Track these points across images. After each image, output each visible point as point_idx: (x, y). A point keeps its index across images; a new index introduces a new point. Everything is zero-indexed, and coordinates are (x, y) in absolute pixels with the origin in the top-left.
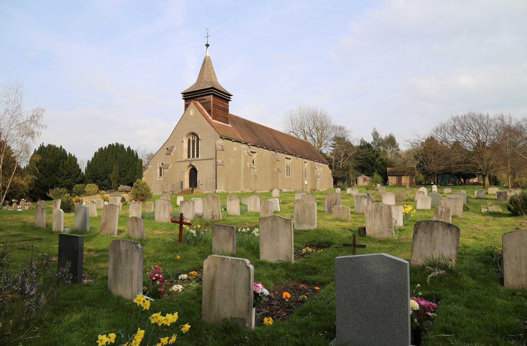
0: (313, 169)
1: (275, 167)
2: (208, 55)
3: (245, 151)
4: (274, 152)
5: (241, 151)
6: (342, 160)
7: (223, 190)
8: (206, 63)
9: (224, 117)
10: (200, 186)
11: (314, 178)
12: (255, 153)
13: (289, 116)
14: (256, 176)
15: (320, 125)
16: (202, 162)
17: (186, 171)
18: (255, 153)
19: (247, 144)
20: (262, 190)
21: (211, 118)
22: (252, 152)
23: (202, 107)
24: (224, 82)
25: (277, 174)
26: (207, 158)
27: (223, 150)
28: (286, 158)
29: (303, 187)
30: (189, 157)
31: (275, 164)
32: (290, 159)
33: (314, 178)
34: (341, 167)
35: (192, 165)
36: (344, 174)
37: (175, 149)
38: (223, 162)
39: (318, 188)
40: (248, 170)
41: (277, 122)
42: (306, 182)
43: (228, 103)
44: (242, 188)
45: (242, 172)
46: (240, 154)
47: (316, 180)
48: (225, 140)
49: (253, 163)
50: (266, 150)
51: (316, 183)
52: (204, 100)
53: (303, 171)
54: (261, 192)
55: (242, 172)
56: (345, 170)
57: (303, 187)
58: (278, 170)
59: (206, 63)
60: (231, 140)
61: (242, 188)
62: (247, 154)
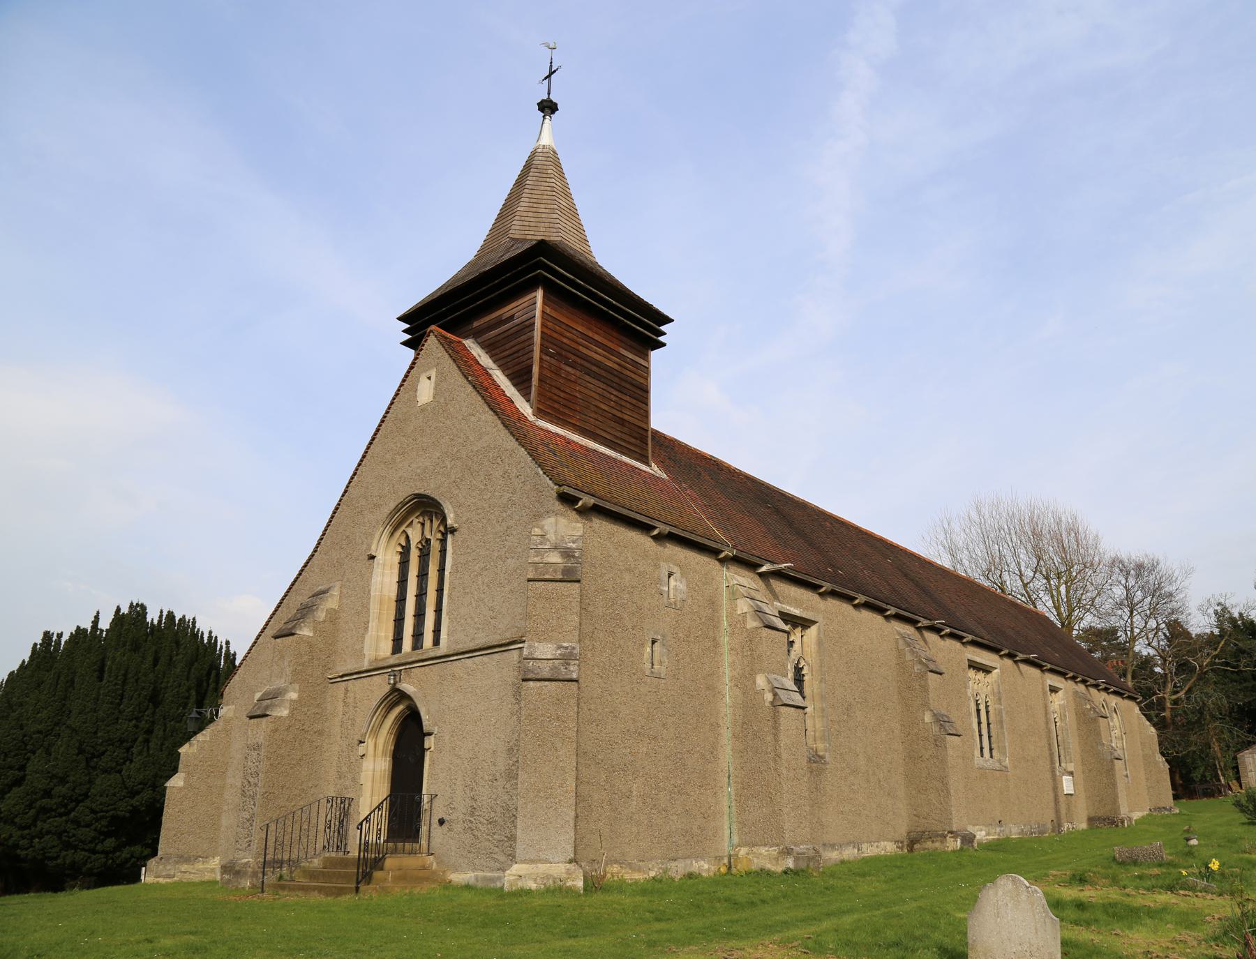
0: (1090, 722)
1: (925, 705)
2: (546, 140)
3: (743, 606)
4: (909, 630)
5: (713, 603)
6: (1170, 687)
7: (559, 869)
8: (540, 173)
9: (622, 422)
10: (438, 831)
11: (1101, 768)
12: (805, 624)
13: (942, 537)
14: (816, 759)
15: (1066, 560)
16: (458, 667)
17: (375, 732)
18: (805, 624)
19: (752, 566)
20: (857, 845)
21: (526, 409)
22: (785, 617)
23: (485, 360)
24: (623, 253)
25: (938, 743)
26: (482, 640)
27: (570, 577)
28: (974, 666)
29: (1057, 812)
30: (397, 648)
31: (925, 688)
32: (986, 670)
33: (1101, 768)
34: (1167, 714)
35: (402, 696)
36: (1188, 744)
37: (331, 602)
38: (567, 658)
39: (1124, 811)
40: (761, 721)
41: (907, 491)
42: (1067, 785)
43: (646, 357)
44: (727, 837)
45: (726, 734)
46: (713, 621)
47: (1111, 771)
48: (599, 524)
49: (799, 680)
50: (866, 614)
51: (1114, 785)
52: (501, 322)
53: (1049, 731)
54: (849, 853)
55: (726, 734)
56: (1190, 726)
57: (1057, 812)
58: (941, 720)
59: (540, 173)
60: (645, 528)
61: (727, 837)
62: (752, 623)
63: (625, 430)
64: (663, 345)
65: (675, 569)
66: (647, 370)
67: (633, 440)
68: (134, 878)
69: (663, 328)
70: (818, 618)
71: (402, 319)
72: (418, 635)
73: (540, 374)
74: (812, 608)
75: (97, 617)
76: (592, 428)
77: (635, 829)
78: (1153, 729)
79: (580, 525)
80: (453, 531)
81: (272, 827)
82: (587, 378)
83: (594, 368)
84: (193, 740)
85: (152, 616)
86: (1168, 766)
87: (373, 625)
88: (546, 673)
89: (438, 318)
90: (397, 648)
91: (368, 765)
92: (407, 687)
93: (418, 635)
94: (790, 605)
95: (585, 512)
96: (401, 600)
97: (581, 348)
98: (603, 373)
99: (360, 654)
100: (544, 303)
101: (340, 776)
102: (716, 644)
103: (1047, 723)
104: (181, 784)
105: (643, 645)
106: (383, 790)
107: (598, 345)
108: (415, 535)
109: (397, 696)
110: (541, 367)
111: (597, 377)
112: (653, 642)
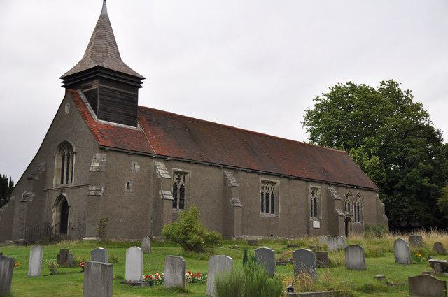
30: (62, 183)
66: (137, 96)
69: (63, 84)
72: (67, 180)
89: (71, 81)
90: (62, 183)
92: (64, 194)
93: (67, 180)
96: (63, 169)
101: (47, 217)
102: (149, 181)
106: (59, 220)
108: (66, 153)
109: (61, 197)
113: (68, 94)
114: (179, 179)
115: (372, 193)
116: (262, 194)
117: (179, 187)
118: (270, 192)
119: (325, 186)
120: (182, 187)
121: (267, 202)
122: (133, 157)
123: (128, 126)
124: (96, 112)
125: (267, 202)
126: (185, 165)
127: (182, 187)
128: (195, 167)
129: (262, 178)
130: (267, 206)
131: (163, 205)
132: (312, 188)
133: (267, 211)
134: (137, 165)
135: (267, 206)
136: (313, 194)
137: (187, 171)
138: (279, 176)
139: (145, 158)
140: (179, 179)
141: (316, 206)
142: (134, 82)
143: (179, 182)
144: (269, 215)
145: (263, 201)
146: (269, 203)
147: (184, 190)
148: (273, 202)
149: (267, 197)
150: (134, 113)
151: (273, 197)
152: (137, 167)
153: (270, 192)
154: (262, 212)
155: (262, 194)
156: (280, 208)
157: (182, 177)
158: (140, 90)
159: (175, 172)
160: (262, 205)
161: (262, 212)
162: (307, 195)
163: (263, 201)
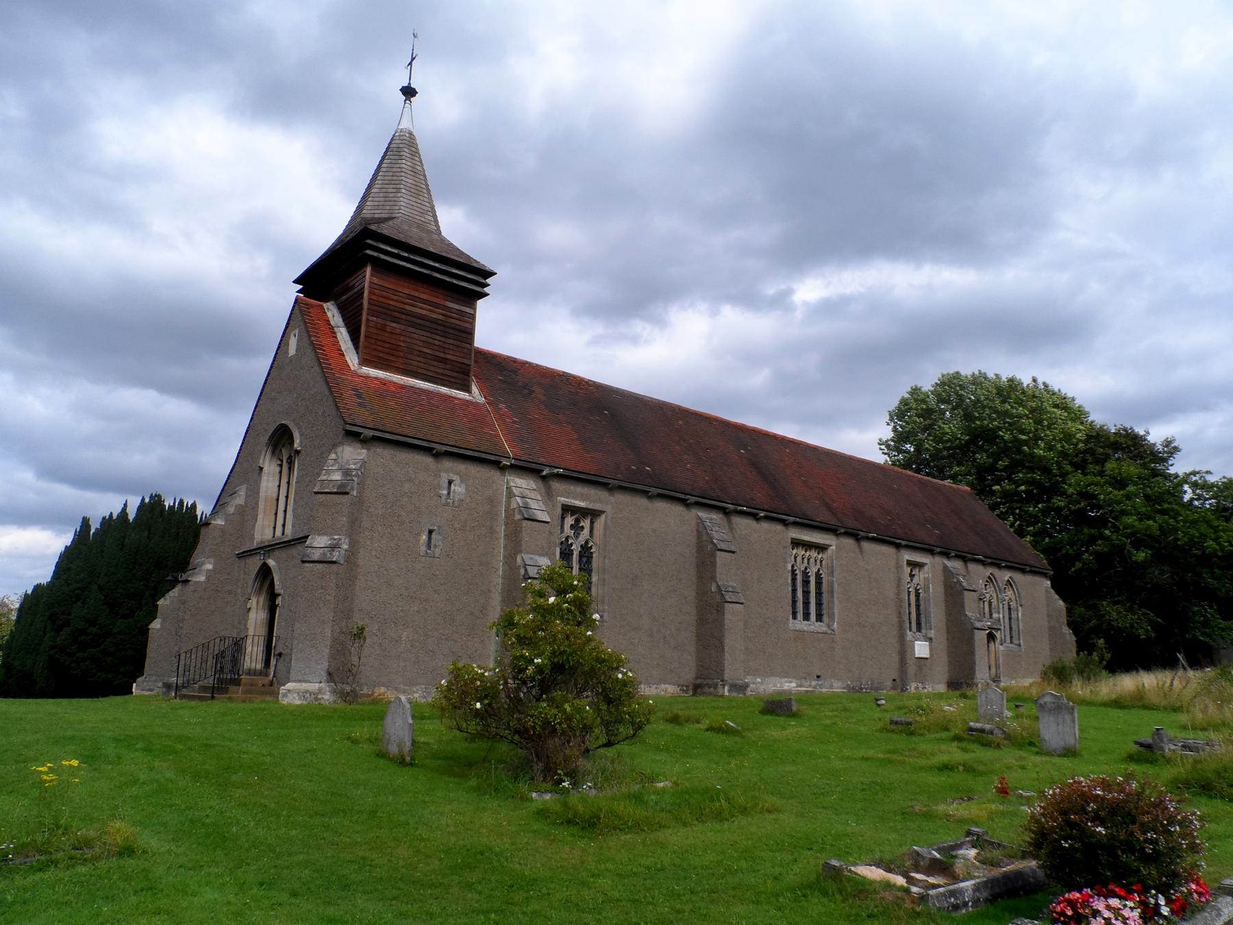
1: (713, 578)
5: (492, 501)
18: (594, 514)
28: (796, 543)
63: (448, 367)
64: (487, 295)
65: (455, 477)
66: (473, 316)
67: (455, 374)
68: (129, 691)
69: (488, 281)
70: (608, 508)
71: (296, 282)
73: (367, 331)
74: (600, 501)
75: (125, 505)
76: (414, 369)
77: (402, 664)
78: (1061, 602)
79: (364, 451)
80: (298, 452)
81: (182, 657)
82: (412, 330)
83: (419, 321)
84: (167, 596)
85: (168, 503)
86: (1074, 638)
87: (260, 517)
88: (316, 557)
91: (252, 615)
94: (575, 498)
95: (365, 442)
97: (407, 307)
98: (428, 324)
99: (252, 538)
100: (372, 275)
102: (492, 531)
103: (898, 594)
104: (159, 626)
105: (419, 534)
107: (423, 304)
110: (367, 326)
111: (420, 327)
112: (430, 532)
113: (297, 311)
114: (576, 527)
115: (1037, 579)
116: (793, 571)
117: (576, 549)
118: (813, 571)
119: (939, 561)
120: (585, 549)
121: (806, 593)
122: (447, 464)
123: (444, 390)
124: (356, 347)
125: (806, 593)
126: (602, 494)
127: (585, 549)
128: (621, 498)
129: (795, 533)
130: (806, 604)
131: (435, 216)
132: (910, 563)
133: (806, 616)
134: (459, 482)
135: (806, 604)
136: (912, 576)
137: (598, 507)
138: (832, 530)
139: (401, 237)
140: (576, 527)
141: (918, 606)
142: (465, 281)
143: (577, 536)
144: (813, 626)
145: (794, 591)
146: (810, 597)
147: (590, 557)
148: (819, 594)
149: (806, 582)
150: (458, 357)
151: (918, 595)
152: (459, 489)
153: (813, 571)
154: (795, 617)
155: (793, 571)
156: (836, 611)
157: (586, 523)
158: (480, 303)
159: (567, 509)
160: (794, 602)
161: (795, 617)
162: (899, 580)
163: (794, 591)
